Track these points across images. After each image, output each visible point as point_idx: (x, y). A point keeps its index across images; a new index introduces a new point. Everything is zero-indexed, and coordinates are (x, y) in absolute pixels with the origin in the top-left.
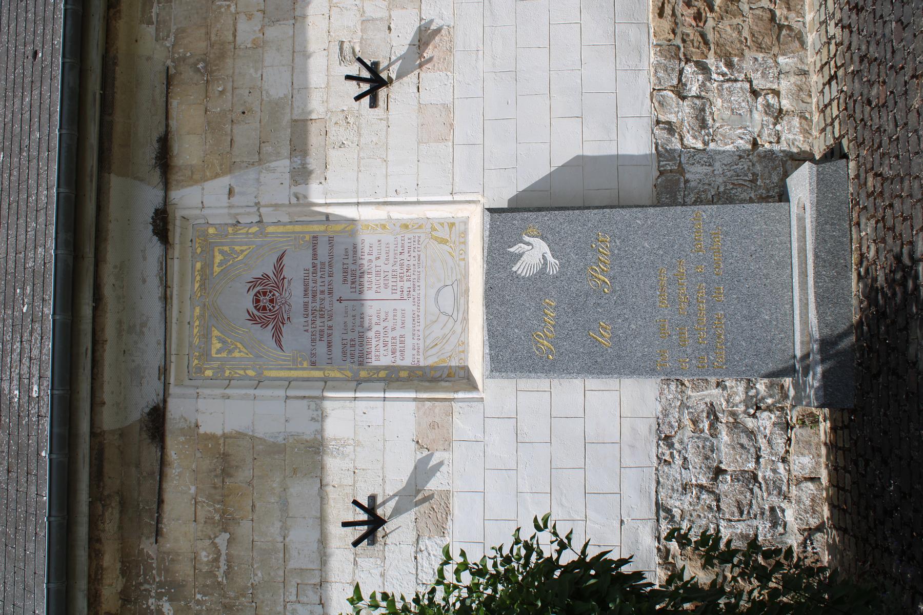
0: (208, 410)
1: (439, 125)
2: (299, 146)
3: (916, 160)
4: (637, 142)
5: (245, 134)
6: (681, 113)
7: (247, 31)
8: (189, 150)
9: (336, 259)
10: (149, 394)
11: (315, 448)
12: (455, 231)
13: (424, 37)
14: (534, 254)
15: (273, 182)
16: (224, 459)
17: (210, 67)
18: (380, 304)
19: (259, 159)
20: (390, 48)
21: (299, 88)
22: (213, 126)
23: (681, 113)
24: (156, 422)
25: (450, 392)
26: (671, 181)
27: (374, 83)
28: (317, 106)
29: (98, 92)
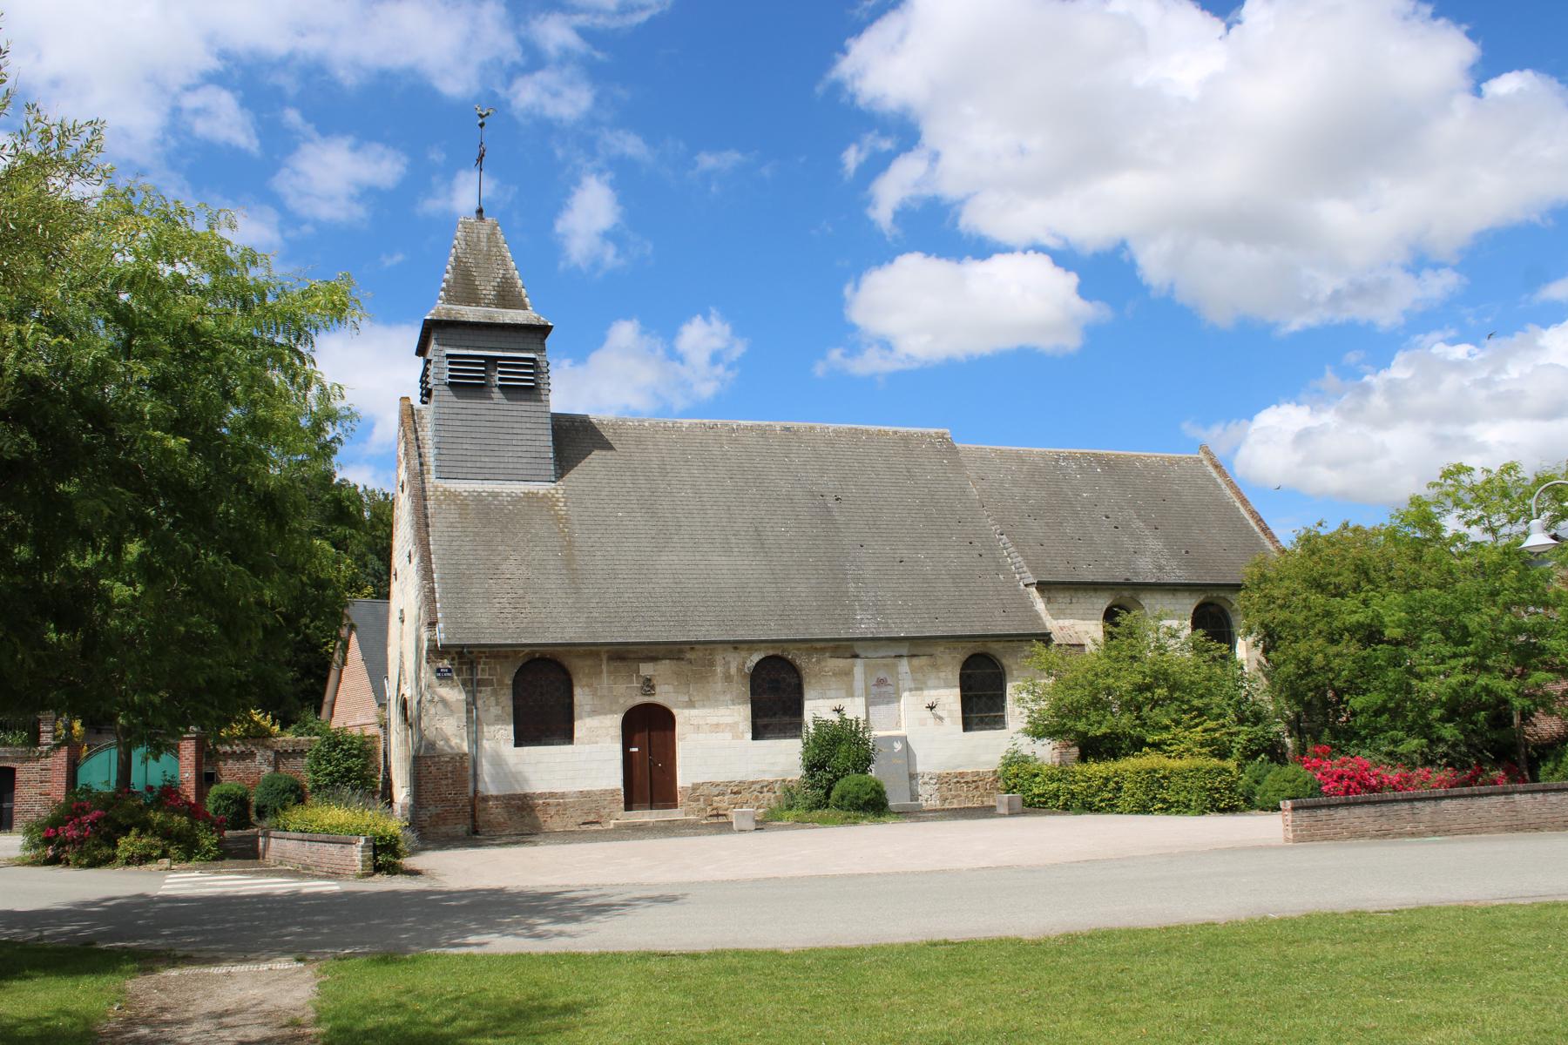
0: (859, 668)
1: (923, 723)
2: (917, 689)
3: (797, 1041)
4: (920, 769)
5: (919, 676)
6: (926, 779)
7: (942, 675)
8: (916, 661)
9: (894, 697)
10: (863, 654)
11: (852, 695)
12: (898, 725)
13: (941, 718)
14: (898, 746)
15: (909, 683)
16: (848, 673)
17: (934, 666)
18: (882, 708)
19: (914, 680)
20: (938, 711)
21: (929, 688)
22: (921, 667)
23: (926, 779)
24: (856, 656)
25: (308, 897)
26: (913, 777)
27: (931, 708)
28: (926, 692)
29: (500, 320)
